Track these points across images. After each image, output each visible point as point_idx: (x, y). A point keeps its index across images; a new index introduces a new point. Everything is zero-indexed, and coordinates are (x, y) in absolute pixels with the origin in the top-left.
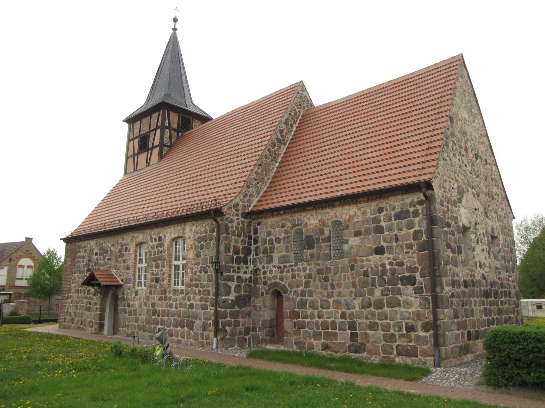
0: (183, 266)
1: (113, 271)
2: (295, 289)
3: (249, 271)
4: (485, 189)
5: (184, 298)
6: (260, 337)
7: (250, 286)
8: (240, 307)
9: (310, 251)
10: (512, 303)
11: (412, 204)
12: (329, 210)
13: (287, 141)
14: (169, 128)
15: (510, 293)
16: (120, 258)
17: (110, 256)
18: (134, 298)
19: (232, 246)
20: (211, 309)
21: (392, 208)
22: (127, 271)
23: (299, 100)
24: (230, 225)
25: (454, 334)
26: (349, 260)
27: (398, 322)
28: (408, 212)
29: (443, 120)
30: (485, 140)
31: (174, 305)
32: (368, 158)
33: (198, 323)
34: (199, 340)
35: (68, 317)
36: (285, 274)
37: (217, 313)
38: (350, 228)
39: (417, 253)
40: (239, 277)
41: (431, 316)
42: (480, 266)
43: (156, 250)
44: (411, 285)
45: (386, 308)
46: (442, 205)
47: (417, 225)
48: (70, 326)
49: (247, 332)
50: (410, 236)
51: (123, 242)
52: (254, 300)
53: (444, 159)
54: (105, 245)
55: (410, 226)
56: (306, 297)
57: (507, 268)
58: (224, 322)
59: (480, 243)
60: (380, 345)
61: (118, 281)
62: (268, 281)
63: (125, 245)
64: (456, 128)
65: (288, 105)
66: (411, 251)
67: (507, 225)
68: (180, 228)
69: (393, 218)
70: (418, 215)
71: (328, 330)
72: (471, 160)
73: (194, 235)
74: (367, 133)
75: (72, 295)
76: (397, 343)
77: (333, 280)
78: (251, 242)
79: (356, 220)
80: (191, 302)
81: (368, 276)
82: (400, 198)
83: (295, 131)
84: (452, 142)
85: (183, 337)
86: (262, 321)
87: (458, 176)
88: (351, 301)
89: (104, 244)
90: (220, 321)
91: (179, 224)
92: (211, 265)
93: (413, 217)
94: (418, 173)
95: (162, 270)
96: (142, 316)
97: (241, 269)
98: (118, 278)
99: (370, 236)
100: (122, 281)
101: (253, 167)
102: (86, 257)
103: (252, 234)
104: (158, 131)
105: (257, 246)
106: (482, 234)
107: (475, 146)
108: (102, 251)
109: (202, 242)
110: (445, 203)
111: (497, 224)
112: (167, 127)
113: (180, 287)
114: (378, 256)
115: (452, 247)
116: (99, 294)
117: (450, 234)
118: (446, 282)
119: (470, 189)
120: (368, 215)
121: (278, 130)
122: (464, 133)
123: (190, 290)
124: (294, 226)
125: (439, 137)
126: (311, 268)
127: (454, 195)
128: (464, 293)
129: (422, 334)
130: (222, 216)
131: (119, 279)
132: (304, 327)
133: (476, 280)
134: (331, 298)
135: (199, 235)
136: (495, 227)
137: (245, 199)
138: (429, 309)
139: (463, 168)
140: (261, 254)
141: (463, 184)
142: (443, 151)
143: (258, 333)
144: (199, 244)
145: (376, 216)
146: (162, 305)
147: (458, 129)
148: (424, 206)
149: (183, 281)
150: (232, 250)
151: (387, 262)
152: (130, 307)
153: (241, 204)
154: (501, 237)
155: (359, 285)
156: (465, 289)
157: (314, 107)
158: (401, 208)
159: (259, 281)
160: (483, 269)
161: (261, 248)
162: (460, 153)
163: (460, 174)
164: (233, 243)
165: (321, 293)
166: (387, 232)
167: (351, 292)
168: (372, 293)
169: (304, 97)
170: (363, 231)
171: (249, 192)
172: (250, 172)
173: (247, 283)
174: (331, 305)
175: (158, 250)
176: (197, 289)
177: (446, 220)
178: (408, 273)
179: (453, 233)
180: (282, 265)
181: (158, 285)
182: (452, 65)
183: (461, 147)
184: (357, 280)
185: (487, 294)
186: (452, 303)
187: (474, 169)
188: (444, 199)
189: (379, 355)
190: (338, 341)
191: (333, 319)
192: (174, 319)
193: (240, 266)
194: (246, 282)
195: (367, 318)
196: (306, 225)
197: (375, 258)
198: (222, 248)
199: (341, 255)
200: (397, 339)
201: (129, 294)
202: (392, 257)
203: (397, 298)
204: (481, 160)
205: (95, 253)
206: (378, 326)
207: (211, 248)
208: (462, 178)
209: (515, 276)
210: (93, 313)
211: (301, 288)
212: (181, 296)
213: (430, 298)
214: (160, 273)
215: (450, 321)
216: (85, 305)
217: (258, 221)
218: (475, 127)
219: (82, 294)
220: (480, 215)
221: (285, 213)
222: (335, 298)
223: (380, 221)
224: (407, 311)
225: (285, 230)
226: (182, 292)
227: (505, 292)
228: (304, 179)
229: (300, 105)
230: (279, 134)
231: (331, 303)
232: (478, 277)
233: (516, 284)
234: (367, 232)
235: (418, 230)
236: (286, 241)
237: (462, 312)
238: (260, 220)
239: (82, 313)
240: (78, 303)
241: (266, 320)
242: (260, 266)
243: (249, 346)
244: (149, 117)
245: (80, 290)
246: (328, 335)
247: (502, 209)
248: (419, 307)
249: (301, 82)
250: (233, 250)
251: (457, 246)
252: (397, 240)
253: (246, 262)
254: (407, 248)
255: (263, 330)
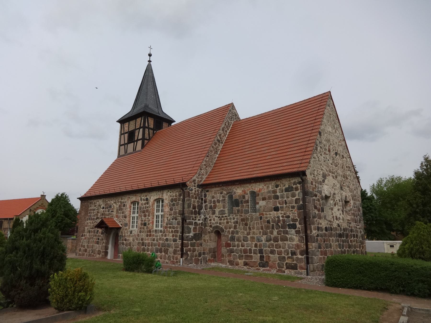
0: (162, 215)
1: (115, 219)
2: (228, 230)
3: (201, 219)
4: (341, 173)
5: (162, 235)
6: (208, 258)
7: (202, 228)
8: (196, 240)
9: (237, 208)
10: (358, 241)
11: (295, 183)
12: (248, 185)
13: (223, 141)
14: (149, 128)
15: (357, 235)
16: (119, 210)
17: (113, 209)
18: (130, 235)
19: (192, 204)
20: (179, 242)
21: (284, 185)
22: (124, 219)
23: (231, 115)
24: (191, 192)
25: (319, 258)
26: (259, 214)
27: (286, 250)
28: (293, 188)
29: (314, 134)
30: (343, 143)
31: (156, 239)
32: (271, 155)
33: (171, 250)
34: (171, 260)
35: (82, 249)
36: (222, 221)
37: (182, 244)
38: (260, 195)
39: (297, 211)
40: (195, 223)
41: (305, 247)
42: (337, 219)
43: (144, 206)
44: (294, 229)
45: (280, 242)
46: (312, 184)
47: (297, 195)
48: (84, 254)
49: (200, 255)
50: (293, 201)
51: (122, 201)
52: (204, 236)
53: (314, 158)
54: (109, 202)
55: (293, 196)
56: (235, 235)
57: (355, 221)
58: (187, 249)
59: (336, 206)
60: (277, 262)
61: (119, 225)
62: (213, 225)
63: (123, 202)
64: (323, 138)
65: (224, 118)
66: (294, 210)
67: (356, 194)
68: (160, 193)
69: (284, 191)
70: (298, 190)
71: (247, 254)
72: (332, 156)
73: (169, 197)
74: (271, 140)
75: (85, 234)
76: (286, 262)
77: (250, 225)
78: (202, 202)
79: (263, 191)
80: (167, 237)
81: (270, 223)
82: (288, 180)
83: (228, 135)
84: (320, 147)
85: (161, 259)
86: (209, 248)
87: (323, 167)
88: (260, 237)
89: (108, 202)
90: (185, 248)
91: (159, 191)
92: (179, 215)
93: (295, 191)
94: (298, 166)
95: (148, 218)
96: (135, 247)
97: (197, 218)
98: (118, 223)
99: (271, 201)
100: (121, 225)
101: (203, 158)
102: (96, 210)
103: (203, 197)
104: (141, 130)
105: (206, 205)
106: (338, 200)
107: (336, 148)
108: (107, 206)
109: (174, 202)
110: (314, 183)
111: (350, 194)
112: (147, 128)
113: (160, 228)
114: (276, 212)
115: (318, 208)
116: (105, 233)
117: (317, 201)
118: (313, 227)
119: (331, 174)
120: (270, 189)
121: (218, 135)
122: (328, 141)
123: (166, 230)
124: (227, 193)
125: (312, 145)
126: (238, 218)
127: (321, 178)
128: (325, 235)
129: (300, 257)
130: (186, 187)
131: (119, 224)
132: (233, 252)
133: (334, 228)
134: (249, 235)
135: (172, 198)
136: (348, 196)
137: (199, 177)
138: (304, 243)
139: (327, 162)
140: (208, 209)
141: (326, 171)
142: (313, 153)
143: (206, 256)
144: (172, 203)
145: (274, 190)
146: (148, 240)
147: (324, 138)
148: (302, 185)
149: (161, 225)
150: (192, 207)
151: (280, 215)
152: (127, 241)
153: (197, 179)
154: (352, 202)
155: (265, 228)
156: (326, 232)
157: (240, 120)
158: (289, 186)
159: (207, 225)
160: (339, 221)
161: (209, 205)
162: (325, 153)
163: (324, 166)
164: (192, 202)
165: (243, 232)
166: (281, 198)
167: (260, 232)
168: (272, 233)
169: (234, 113)
170: (267, 197)
171: (201, 172)
172: (202, 160)
173: (200, 226)
174: (249, 239)
175: (146, 206)
176: (170, 230)
177: (314, 193)
178: (292, 222)
179: (318, 200)
180: (221, 216)
181: (145, 227)
182: (323, 98)
183: (326, 150)
184: (264, 225)
185: (340, 236)
186: (317, 240)
187: (334, 162)
188: (313, 181)
189: (276, 269)
190: (253, 260)
191: (250, 248)
192: (156, 248)
193: (196, 216)
194: (199, 225)
195: (269, 247)
196: (235, 193)
197: (274, 214)
198: (186, 206)
199: (254, 211)
200: (286, 260)
201: (126, 233)
202: (283, 213)
203: (286, 236)
204: (340, 155)
205: (102, 207)
206: (275, 252)
207: (179, 205)
208: (325, 168)
209: (362, 226)
210: (101, 246)
211: (232, 229)
212: (160, 234)
213: (304, 236)
214: (146, 220)
215: (316, 250)
216: (95, 240)
217: (206, 190)
218: (336, 136)
219: (93, 233)
220: (337, 189)
221: (222, 185)
222: (251, 235)
223: (277, 193)
224: (291, 244)
225: (222, 196)
226: (161, 231)
227: (354, 235)
228: (234, 166)
229: (231, 118)
230: (219, 137)
231: (249, 238)
232: (335, 225)
233: (361, 230)
234: (270, 198)
235: (298, 198)
236: (223, 201)
237: (324, 245)
238: (208, 189)
239: (92, 246)
240: (90, 239)
241: (211, 248)
242: (208, 216)
243: (201, 263)
244: (135, 120)
245: (92, 231)
246: (247, 257)
247: (353, 185)
248: (298, 242)
249: (232, 104)
250: (193, 207)
251: (321, 207)
252: (286, 203)
253: (199, 214)
254: (292, 208)
255: (210, 254)
